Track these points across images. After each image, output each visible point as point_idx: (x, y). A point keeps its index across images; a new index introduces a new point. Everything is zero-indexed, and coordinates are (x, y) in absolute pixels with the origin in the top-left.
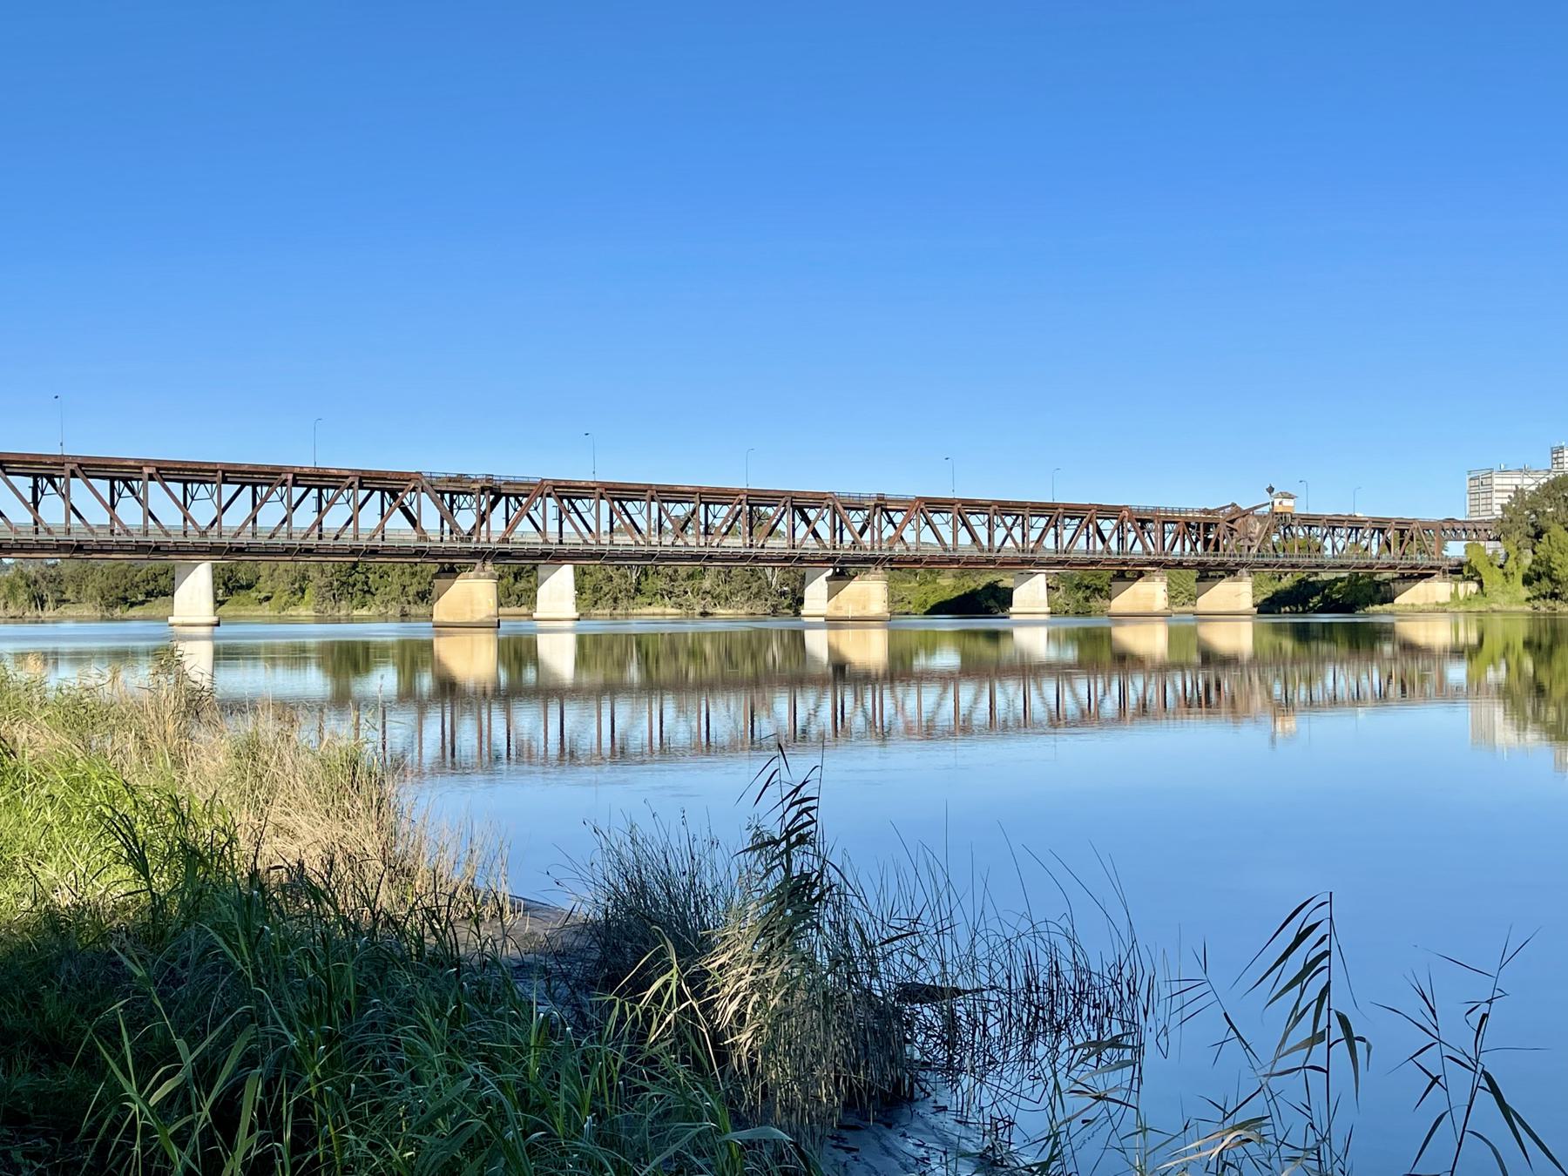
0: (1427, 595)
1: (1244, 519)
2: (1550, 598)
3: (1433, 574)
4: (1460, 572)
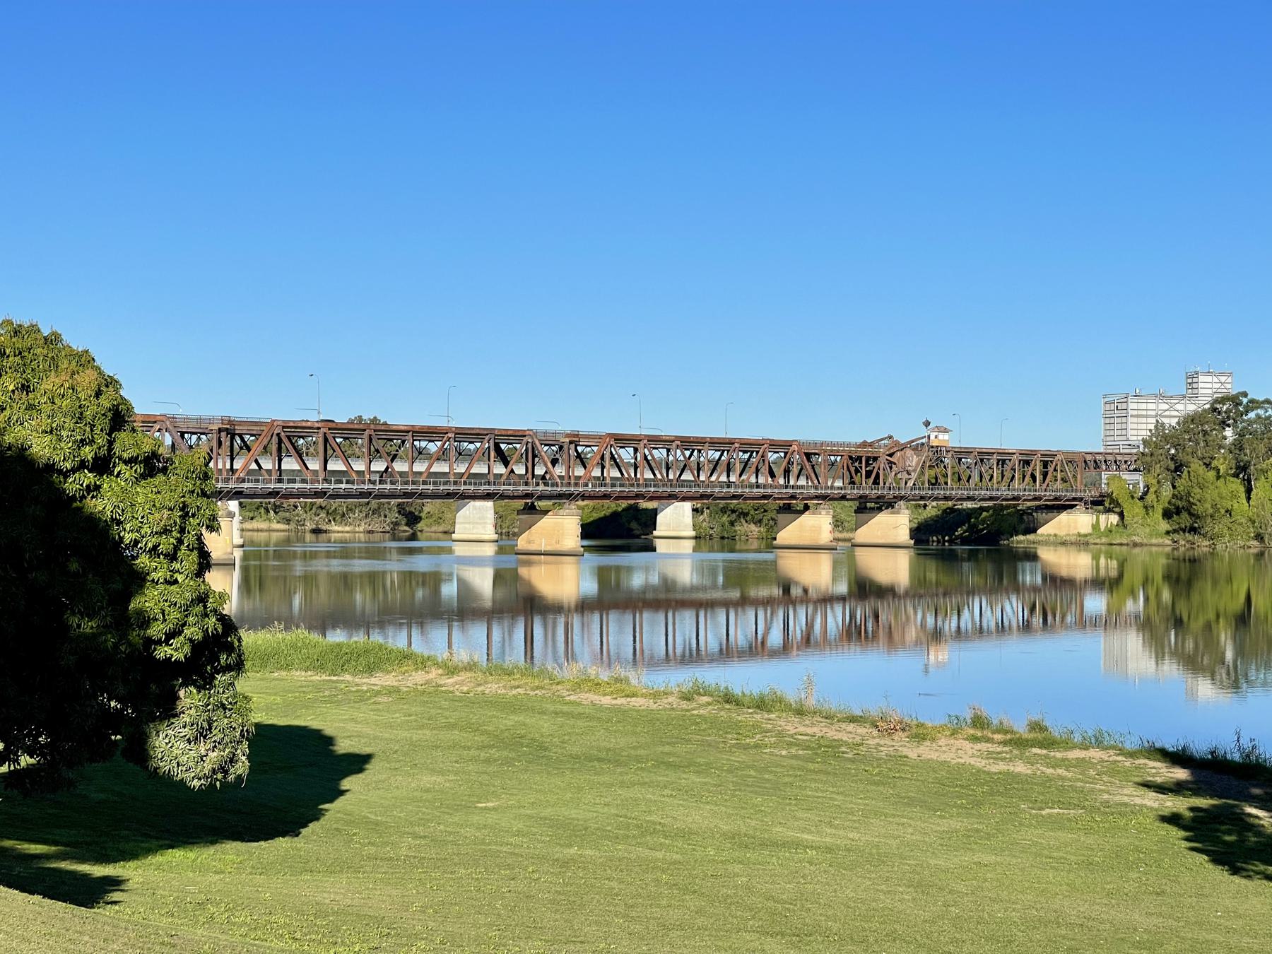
0: (1069, 526)
1: (903, 452)
2: (1189, 532)
3: (1076, 505)
4: (1100, 503)
